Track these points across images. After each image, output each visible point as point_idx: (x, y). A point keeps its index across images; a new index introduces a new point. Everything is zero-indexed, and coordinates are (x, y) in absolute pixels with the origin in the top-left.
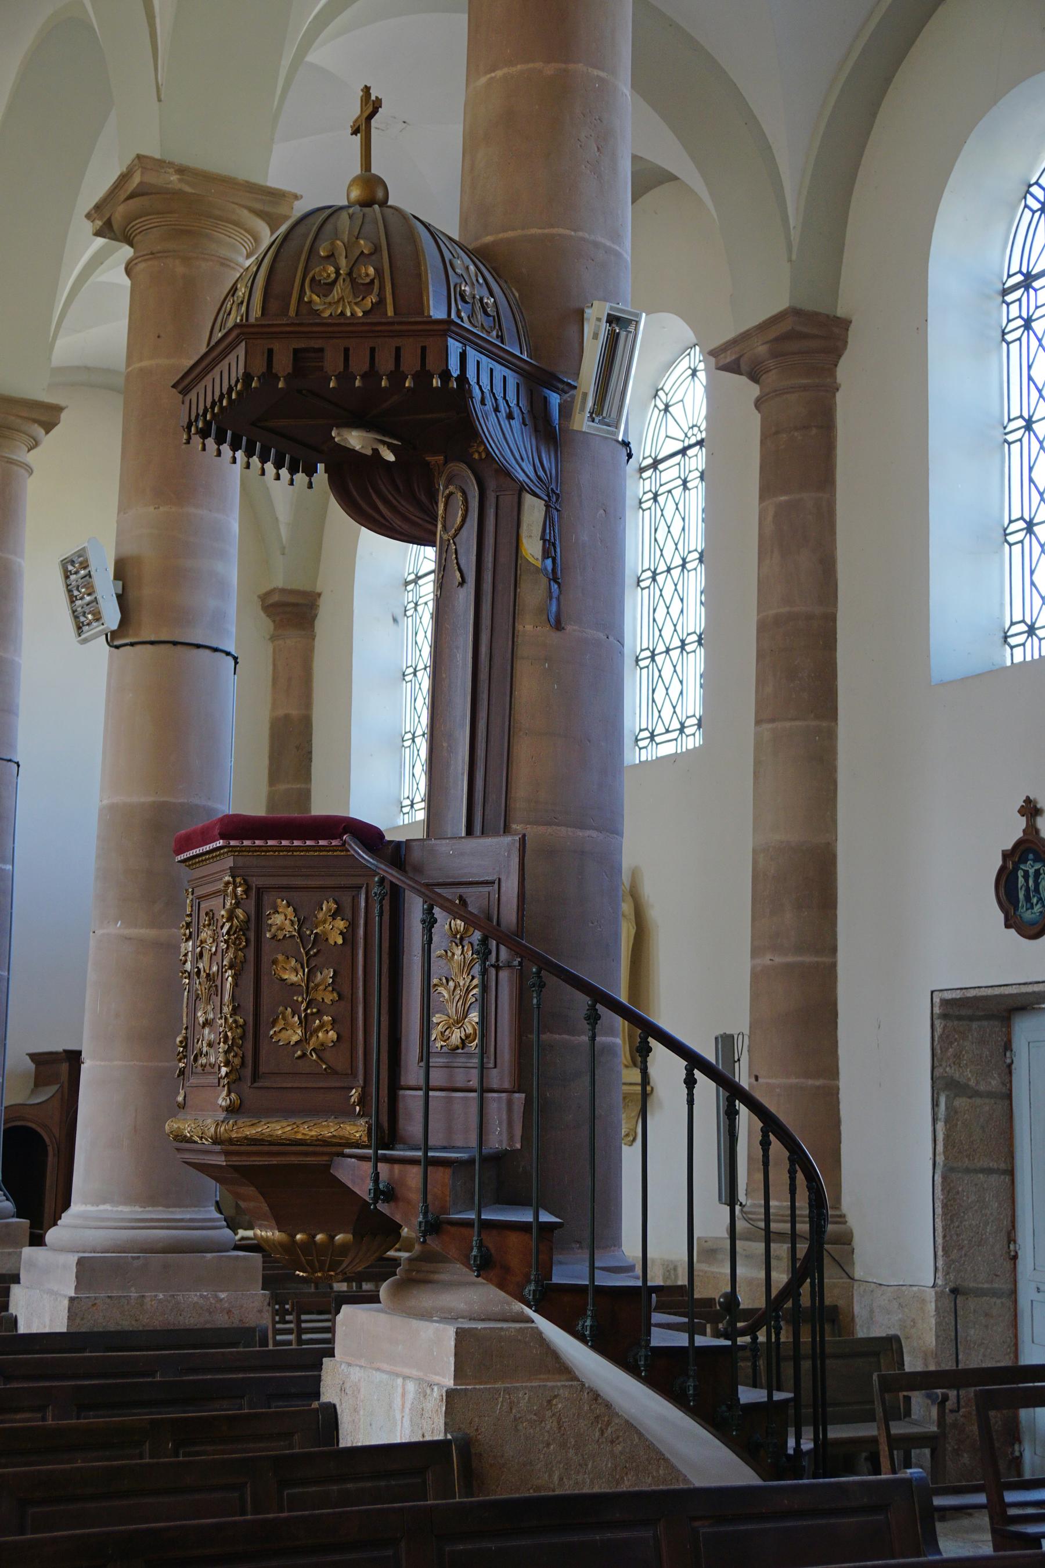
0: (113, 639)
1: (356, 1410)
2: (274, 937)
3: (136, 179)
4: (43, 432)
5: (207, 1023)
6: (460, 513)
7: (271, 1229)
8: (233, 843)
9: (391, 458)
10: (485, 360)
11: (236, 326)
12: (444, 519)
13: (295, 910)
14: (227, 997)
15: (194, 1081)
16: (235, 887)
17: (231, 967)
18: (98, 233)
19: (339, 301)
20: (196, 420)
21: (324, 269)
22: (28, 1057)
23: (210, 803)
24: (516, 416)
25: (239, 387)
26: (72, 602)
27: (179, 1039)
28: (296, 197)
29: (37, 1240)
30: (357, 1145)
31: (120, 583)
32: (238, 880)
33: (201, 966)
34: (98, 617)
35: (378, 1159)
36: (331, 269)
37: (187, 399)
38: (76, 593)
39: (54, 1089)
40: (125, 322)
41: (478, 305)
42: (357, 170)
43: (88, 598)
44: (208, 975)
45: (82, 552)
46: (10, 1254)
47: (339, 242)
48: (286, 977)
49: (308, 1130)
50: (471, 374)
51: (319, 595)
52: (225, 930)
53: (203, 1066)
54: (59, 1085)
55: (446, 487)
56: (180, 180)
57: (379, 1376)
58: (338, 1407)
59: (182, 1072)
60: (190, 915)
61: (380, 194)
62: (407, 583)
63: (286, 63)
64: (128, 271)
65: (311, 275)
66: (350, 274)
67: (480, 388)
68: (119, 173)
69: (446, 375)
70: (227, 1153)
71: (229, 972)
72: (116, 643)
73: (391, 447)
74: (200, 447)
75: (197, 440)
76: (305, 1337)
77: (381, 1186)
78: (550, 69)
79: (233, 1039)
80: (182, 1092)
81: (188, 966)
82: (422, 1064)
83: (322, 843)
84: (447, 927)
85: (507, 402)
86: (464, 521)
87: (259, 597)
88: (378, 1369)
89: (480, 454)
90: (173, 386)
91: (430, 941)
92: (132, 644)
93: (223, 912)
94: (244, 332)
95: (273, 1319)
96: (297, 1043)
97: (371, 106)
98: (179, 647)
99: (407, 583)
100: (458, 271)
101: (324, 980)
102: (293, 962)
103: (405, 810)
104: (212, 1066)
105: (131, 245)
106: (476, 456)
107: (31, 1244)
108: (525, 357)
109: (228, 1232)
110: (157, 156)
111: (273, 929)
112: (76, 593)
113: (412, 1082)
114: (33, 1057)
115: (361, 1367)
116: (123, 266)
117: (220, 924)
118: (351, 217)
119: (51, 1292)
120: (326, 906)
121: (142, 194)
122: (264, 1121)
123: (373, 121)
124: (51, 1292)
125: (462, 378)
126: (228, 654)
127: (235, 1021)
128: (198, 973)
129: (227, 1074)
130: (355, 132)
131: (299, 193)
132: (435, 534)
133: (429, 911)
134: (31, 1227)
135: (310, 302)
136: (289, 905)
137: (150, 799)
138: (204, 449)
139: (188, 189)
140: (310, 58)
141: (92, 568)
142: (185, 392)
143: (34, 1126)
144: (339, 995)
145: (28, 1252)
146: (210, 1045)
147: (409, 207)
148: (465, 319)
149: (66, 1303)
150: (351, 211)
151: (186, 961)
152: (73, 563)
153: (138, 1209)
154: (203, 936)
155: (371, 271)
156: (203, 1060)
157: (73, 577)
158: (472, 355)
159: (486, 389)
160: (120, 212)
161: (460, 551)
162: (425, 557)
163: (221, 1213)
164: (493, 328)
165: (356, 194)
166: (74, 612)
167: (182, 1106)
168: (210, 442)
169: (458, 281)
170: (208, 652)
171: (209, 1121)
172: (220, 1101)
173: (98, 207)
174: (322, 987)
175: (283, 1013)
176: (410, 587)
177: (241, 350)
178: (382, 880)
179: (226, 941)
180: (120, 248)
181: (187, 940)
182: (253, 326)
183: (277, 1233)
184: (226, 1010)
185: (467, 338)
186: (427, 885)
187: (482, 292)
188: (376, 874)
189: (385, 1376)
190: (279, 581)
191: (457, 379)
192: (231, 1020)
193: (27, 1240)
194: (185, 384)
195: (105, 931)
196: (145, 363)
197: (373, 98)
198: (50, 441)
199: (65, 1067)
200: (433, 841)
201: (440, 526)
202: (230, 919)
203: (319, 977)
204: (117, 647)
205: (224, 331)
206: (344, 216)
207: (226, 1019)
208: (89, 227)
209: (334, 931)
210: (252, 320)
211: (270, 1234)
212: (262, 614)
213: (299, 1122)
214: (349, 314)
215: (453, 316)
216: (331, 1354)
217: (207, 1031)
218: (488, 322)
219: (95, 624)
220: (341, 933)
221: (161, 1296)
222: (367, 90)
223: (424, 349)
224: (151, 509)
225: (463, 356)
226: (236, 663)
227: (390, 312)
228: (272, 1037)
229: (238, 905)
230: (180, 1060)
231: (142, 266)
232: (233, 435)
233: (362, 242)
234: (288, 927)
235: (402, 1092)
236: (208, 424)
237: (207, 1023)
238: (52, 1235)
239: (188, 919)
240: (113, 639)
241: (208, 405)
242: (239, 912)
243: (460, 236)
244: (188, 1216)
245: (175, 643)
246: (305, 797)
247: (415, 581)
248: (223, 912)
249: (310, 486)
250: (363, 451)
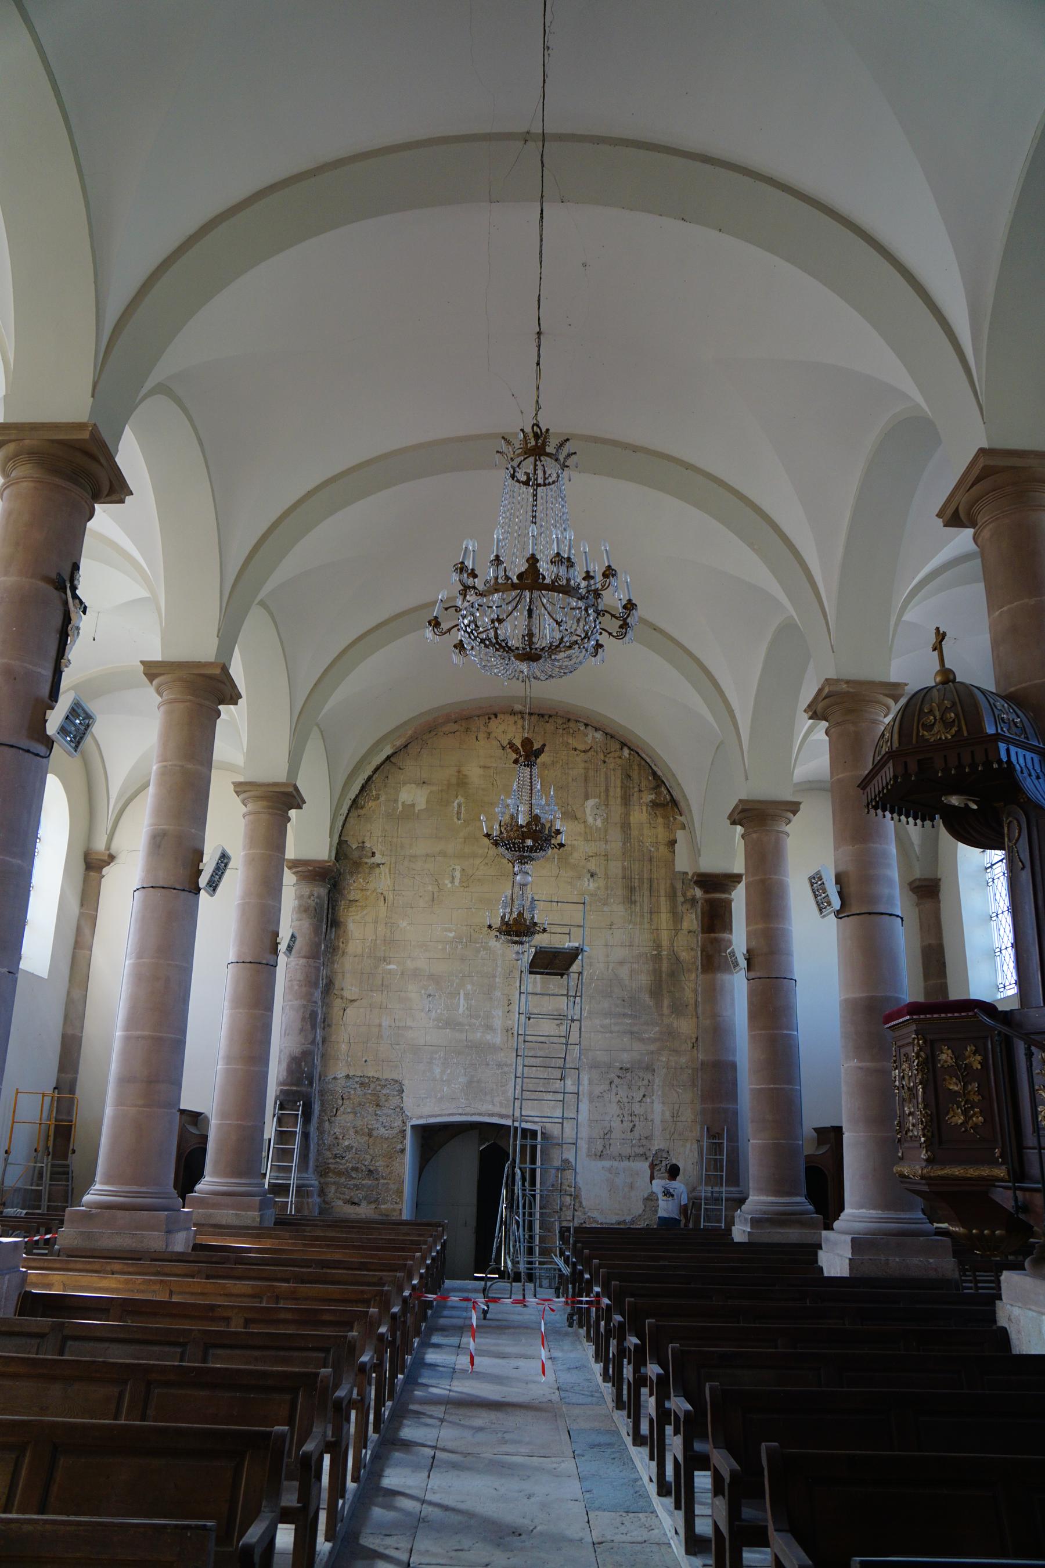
0: (838, 914)
1: (1019, 1332)
2: (942, 1066)
3: (826, 690)
4: (792, 815)
5: (910, 1114)
6: (1017, 831)
7: (958, 1226)
8: (915, 1017)
9: (975, 807)
10: (1019, 750)
11: (887, 753)
12: (1009, 835)
13: (952, 1051)
14: (920, 1100)
15: (906, 1145)
16: (918, 1040)
17: (921, 1083)
18: (810, 718)
19: (937, 733)
20: (871, 802)
21: (928, 718)
22: (813, 1130)
23: (897, 995)
24: (1041, 777)
25: (892, 782)
26: (816, 898)
27: (896, 1123)
28: (906, 685)
29: (829, 1227)
30: (1002, 1180)
31: (839, 886)
32: (920, 1036)
33: (904, 1083)
34: (829, 904)
35: (1016, 1189)
36: (932, 718)
37: (865, 791)
38: (817, 893)
39: (828, 1146)
40: (828, 756)
41: (1012, 724)
42: (938, 668)
43: (823, 895)
44: (908, 1088)
45: (818, 873)
46: (815, 1233)
47: (934, 704)
48: (951, 1088)
49: (973, 1172)
50: (1013, 759)
51: (940, 880)
52: (915, 1064)
53: (911, 1137)
54: (829, 1145)
55: (1007, 819)
56: (848, 687)
57: (1030, 1314)
58: (1008, 1329)
59: (899, 1140)
60: (895, 1056)
61: (951, 677)
62: (987, 869)
63: (892, 623)
64: (827, 733)
65: (921, 723)
66: (941, 718)
67: (1019, 765)
68: (817, 689)
69: (1000, 762)
70: (929, 1185)
71: (920, 1086)
72: (840, 916)
73: (975, 802)
74: (874, 814)
75: (872, 811)
76: (979, 1285)
77: (1019, 1204)
78: (1032, 601)
79: (926, 1122)
80: (900, 1151)
81: (897, 1083)
82: (1035, 1135)
83: (963, 1014)
84: (1040, 1057)
85: (1035, 770)
86: (1020, 835)
87: (908, 884)
88: (1030, 1309)
89: (1023, 798)
90: (858, 786)
91: (1031, 1065)
92: (848, 916)
93: (913, 1054)
94: (891, 755)
95: (960, 1274)
96: (961, 1124)
97: (941, 636)
98: (872, 916)
99: (987, 869)
100: (999, 708)
101: (973, 1089)
102: (954, 1080)
103: (1001, 990)
104: (916, 1137)
105: (827, 721)
106: (1022, 800)
107: (825, 1229)
108: (1041, 746)
109: (930, 1225)
110: (836, 678)
111: (942, 1062)
112: (817, 893)
113: (1031, 1145)
114: (815, 1129)
115: (1019, 1307)
116: (824, 731)
117: (912, 1060)
118: (938, 690)
119: (838, 1255)
120: (970, 1048)
121: (830, 697)
122: (948, 1167)
123: (943, 643)
124: (838, 1255)
125: (1009, 761)
126: (898, 916)
127: (926, 1113)
128: (903, 1087)
129: (924, 1141)
130: (934, 650)
131: (906, 682)
132: (1004, 843)
133: (1028, 1049)
134: (824, 1219)
135: (923, 736)
136: (948, 1048)
137: (864, 995)
138: (876, 815)
139: (851, 690)
140: (904, 619)
141: (824, 880)
142: (864, 788)
143: (820, 1166)
144: (982, 1097)
145: (824, 1233)
146: (913, 1125)
147: (968, 681)
148: (1006, 731)
149: (847, 1261)
150: (938, 687)
151: (895, 1081)
152: (814, 878)
153: (880, 1212)
154: (904, 1067)
155: (953, 715)
156: (911, 1134)
157: (815, 885)
158: (1013, 749)
159: (1023, 765)
160: (820, 707)
161: (1020, 851)
162: (997, 855)
163: (925, 1215)
164: (1022, 734)
165: (938, 679)
166: (817, 902)
167: (902, 1159)
168: (879, 811)
169: (999, 713)
170: (887, 916)
171: (917, 1167)
172: (922, 1156)
173: (809, 706)
174: (972, 1093)
175: (952, 1108)
176: (989, 870)
177: (890, 764)
178: (1000, 1033)
179: (917, 1070)
180: (819, 723)
181: (895, 1069)
182: (895, 751)
183: (962, 1229)
184: (920, 1106)
185: (1008, 741)
186: (1026, 1034)
187: (1012, 716)
188: (996, 1030)
189: (1035, 1314)
190: (917, 874)
191: (1006, 762)
192: (923, 1112)
193: (822, 1226)
194: (864, 784)
195: (848, 1065)
196: (839, 776)
197: (941, 632)
198: (796, 819)
199: (832, 1135)
200: (1026, 1010)
201: (1006, 839)
202: (917, 1058)
203: (970, 1087)
204: (841, 918)
205: (880, 756)
206: (935, 690)
207: (921, 1111)
208: (806, 716)
209: (976, 1061)
210: (894, 749)
211: (957, 1229)
212: (910, 892)
213: (967, 1167)
214: (944, 738)
215: (999, 731)
216: (1001, 1299)
217: (911, 1118)
218: (1018, 731)
219: (828, 908)
220: (980, 1063)
221: (897, 1260)
222: (938, 629)
223: (986, 750)
224: (851, 847)
225: (1008, 751)
226: (902, 921)
227: (965, 734)
228: (947, 1121)
229: (921, 1050)
230: (898, 1134)
231: (833, 730)
232: (906, 810)
233: (946, 702)
234: (950, 1061)
235: (1025, 1151)
236: (877, 803)
237: (910, 1114)
238: (836, 1225)
239: (894, 1058)
240: (838, 915)
241: (877, 793)
242: (922, 1054)
243: (996, 690)
244: (908, 1217)
245: (870, 913)
246: (944, 988)
247: (991, 867)
248: (913, 1054)
249: (933, 826)
250: (960, 806)
